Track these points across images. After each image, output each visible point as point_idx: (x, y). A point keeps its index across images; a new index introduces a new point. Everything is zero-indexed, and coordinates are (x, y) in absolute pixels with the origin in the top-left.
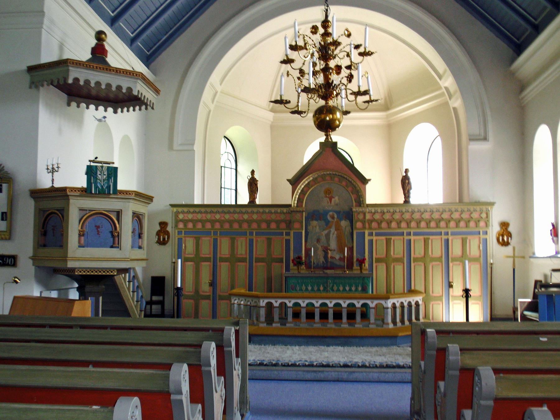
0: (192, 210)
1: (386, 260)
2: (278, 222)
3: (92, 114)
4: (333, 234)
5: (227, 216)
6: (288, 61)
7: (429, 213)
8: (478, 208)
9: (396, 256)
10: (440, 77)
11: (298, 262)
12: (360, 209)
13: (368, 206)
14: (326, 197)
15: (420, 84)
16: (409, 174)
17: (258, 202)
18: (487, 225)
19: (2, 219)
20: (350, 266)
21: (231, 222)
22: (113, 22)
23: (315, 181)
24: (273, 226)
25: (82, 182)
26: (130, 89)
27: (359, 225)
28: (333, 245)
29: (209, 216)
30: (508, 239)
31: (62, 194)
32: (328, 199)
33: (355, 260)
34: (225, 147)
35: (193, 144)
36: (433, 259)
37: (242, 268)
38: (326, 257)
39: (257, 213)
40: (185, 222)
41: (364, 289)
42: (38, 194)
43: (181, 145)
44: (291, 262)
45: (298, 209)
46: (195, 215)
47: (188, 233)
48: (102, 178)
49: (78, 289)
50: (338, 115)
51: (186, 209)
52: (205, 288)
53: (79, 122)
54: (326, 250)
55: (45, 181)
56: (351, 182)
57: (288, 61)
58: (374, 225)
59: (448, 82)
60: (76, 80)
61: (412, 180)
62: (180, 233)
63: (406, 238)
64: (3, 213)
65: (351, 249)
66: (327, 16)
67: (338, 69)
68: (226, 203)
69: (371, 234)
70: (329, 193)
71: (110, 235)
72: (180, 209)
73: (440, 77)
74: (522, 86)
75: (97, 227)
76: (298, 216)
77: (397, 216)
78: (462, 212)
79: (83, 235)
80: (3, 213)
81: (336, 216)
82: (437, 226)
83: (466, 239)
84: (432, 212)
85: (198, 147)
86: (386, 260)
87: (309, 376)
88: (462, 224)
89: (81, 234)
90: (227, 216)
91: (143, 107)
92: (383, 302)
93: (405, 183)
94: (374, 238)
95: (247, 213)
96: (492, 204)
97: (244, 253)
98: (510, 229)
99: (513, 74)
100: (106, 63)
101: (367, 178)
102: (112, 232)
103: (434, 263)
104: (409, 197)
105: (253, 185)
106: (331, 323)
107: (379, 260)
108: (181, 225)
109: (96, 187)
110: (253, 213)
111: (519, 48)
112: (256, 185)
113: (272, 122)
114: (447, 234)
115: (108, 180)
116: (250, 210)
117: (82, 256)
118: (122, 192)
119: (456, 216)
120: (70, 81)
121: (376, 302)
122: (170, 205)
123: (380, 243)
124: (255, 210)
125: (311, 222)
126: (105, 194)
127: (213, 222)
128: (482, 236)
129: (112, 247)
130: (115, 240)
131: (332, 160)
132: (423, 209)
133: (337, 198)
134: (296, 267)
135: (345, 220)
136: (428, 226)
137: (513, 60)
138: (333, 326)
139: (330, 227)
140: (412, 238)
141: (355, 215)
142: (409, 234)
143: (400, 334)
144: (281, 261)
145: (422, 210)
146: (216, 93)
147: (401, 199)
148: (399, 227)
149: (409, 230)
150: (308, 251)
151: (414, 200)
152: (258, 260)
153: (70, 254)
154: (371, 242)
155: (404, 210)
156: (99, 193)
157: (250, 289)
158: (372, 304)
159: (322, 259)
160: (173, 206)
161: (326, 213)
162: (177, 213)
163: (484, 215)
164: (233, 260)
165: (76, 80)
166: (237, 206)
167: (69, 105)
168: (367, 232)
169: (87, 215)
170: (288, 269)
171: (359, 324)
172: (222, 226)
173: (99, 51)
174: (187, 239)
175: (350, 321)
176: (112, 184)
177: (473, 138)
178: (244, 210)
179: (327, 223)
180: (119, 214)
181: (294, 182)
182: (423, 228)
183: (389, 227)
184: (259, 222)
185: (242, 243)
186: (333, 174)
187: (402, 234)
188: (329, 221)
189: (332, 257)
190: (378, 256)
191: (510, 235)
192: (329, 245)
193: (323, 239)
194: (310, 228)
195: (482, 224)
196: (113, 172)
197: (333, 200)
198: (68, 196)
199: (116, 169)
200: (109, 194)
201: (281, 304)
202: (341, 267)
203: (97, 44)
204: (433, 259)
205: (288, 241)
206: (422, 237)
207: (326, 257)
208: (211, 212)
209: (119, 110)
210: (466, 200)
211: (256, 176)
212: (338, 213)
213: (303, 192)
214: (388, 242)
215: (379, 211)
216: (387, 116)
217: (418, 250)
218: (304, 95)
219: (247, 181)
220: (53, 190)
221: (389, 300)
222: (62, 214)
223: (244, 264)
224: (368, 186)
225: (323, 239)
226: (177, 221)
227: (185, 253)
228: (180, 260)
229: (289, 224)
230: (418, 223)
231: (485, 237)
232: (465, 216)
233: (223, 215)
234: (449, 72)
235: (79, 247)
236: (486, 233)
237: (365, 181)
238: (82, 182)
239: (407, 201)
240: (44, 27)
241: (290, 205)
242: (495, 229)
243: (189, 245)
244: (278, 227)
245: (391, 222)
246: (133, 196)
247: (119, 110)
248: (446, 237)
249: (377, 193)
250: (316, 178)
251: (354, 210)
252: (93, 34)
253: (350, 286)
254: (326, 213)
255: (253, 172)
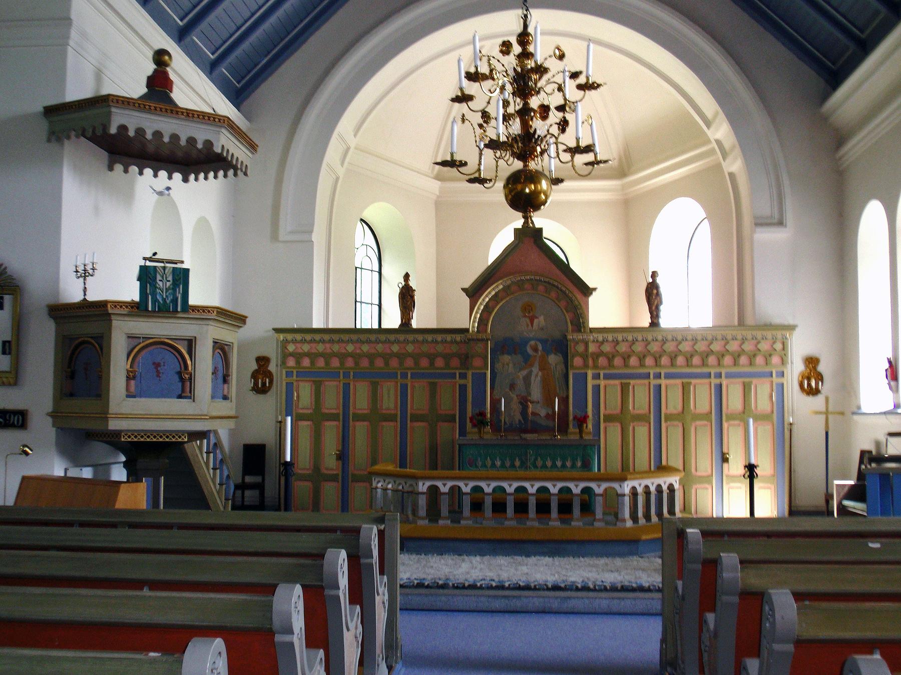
0: (308, 337)
1: (622, 418)
2: (447, 357)
3: (148, 183)
4: (537, 376)
5: (365, 348)
6: (463, 98)
7: (691, 343)
8: (769, 335)
9: (637, 412)
10: (708, 124)
11: (479, 420)
12: (580, 337)
13: (593, 330)
14: (525, 316)
15: (677, 135)
16: (659, 280)
17: (415, 324)
18: (783, 362)
19: (4, 353)
20: (563, 428)
21: (371, 357)
22: (181, 35)
23: (506, 289)
24: (440, 362)
25: (131, 292)
26: (209, 144)
27: (578, 361)
28: (536, 393)
29: (336, 348)
30: (817, 384)
31: (98, 312)
32: (528, 320)
33: (571, 418)
34: (362, 237)
35: (311, 232)
36: (697, 417)
37: (389, 431)
38: (524, 412)
39: (413, 342)
40: (298, 356)
41: (587, 465)
42: (62, 313)
43: (292, 232)
44: (468, 420)
45: (480, 336)
46: (313, 345)
47: (303, 374)
48: (164, 286)
49: (126, 465)
50: (544, 185)
51: (299, 337)
52: (330, 463)
53: (127, 196)
54: (524, 402)
55: (72, 292)
56: (564, 293)
57: (463, 98)
58: (602, 361)
59: (721, 131)
60: (123, 128)
61: (662, 290)
62: (289, 374)
63: (654, 382)
64: (4, 343)
65: (564, 401)
66: (526, 26)
67: (545, 110)
68: (364, 327)
69: (597, 377)
70: (529, 310)
71: (177, 378)
72: (289, 337)
73: (708, 124)
74: (840, 138)
75: (157, 365)
76: (479, 347)
77: (638, 348)
78: (743, 340)
79: (134, 378)
80: (4, 343)
81: (540, 348)
82: (704, 364)
83: (750, 384)
84: (695, 341)
85: (318, 237)
86: (622, 418)
87: (497, 604)
88: (743, 360)
89: (131, 376)
90: (365, 348)
91: (231, 173)
92: (616, 485)
93: (652, 294)
94: (602, 383)
95: (397, 342)
96: (792, 328)
97: (392, 406)
98: (821, 368)
99: (825, 119)
100: (171, 102)
101: (591, 286)
102: (179, 373)
103: (698, 423)
104: (658, 316)
105: (407, 297)
106: (533, 520)
107: (609, 418)
108: (291, 362)
109: (155, 301)
110: (406, 342)
111: (834, 75)
112: (412, 297)
113: (438, 197)
114: (719, 375)
115: (174, 289)
116: (402, 337)
117: (132, 410)
118: (196, 309)
119: (733, 346)
120: (113, 130)
121: (604, 485)
122: (274, 329)
123: (611, 392)
124: (411, 337)
125: (500, 357)
126: (168, 311)
127: (343, 357)
128: (775, 380)
129: (180, 397)
130: (184, 386)
131: (535, 258)
132: (680, 336)
133: (542, 318)
134: (476, 430)
135: (555, 354)
136: (688, 364)
137: (825, 97)
138: (536, 524)
139: (532, 365)
140: (663, 382)
141: (571, 344)
142: (658, 376)
143: (644, 537)
144: (451, 419)
145: (680, 338)
146: (348, 149)
147: (645, 321)
148: (642, 365)
149: (658, 370)
150: (495, 403)
151: (666, 322)
152: (416, 418)
153: (113, 408)
154: (597, 389)
155: (650, 338)
156: (160, 311)
157: (403, 465)
158: (599, 488)
159: (518, 417)
160: (277, 331)
161: (526, 342)
162: (286, 342)
163: (778, 346)
164: (376, 417)
165: (123, 128)
166: (380, 330)
167: (111, 168)
168: (590, 373)
169: (141, 346)
170: (463, 433)
171: (577, 521)
172: (356, 364)
173: (159, 83)
174: (301, 384)
175: (562, 516)
176: (180, 297)
177: (761, 223)
178: (392, 337)
179: (527, 359)
180: (191, 343)
181: (474, 292)
182: (681, 367)
183: (626, 365)
184: (416, 357)
185: (389, 390)
186: (535, 280)
187: (648, 376)
188: (529, 356)
189: (533, 414)
190: (608, 412)
191: (820, 377)
192: (530, 394)
193: (520, 383)
194: (498, 366)
195: (775, 360)
196: (182, 277)
197: (536, 321)
198: (109, 315)
199: (186, 271)
200: (176, 311)
201: (452, 488)
202: (550, 430)
203: (155, 71)
204: (697, 417)
205: (463, 388)
206: (678, 381)
207: (524, 412)
208: (340, 341)
209: (192, 177)
210: (749, 321)
211: (412, 283)
212: (544, 342)
213: (487, 309)
214: (624, 389)
215: (610, 339)
216: (623, 187)
217: (672, 402)
218: (488, 153)
219: (398, 291)
220: (85, 305)
221: (626, 483)
222: (99, 345)
223: (392, 424)
224: (592, 300)
225: (520, 383)
226: (285, 355)
227: (297, 406)
228: (289, 419)
229: (465, 360)
230: (673, 358)
231: (780, 380)
232: (748, 347)
233: (358, 345)
234: (722, 115)
235: (128, 396)
236: (782, 374)
237: (587, 291)
238: (131, 292)
239: (654, 323)
240: (71, 43)
241: (467, 330)
242: (796, 367)
243: (305, 394)
244: (447, 365)
245: (629, 357)
246: (214, 315)
247: (192, 177)
248: (718, 381)
249: (607, 310)
250: (509, 286)
251: (570, 337)
252: (150, 54)
253: (564, 460)
254: (526, 342)
255: (407, 277)
